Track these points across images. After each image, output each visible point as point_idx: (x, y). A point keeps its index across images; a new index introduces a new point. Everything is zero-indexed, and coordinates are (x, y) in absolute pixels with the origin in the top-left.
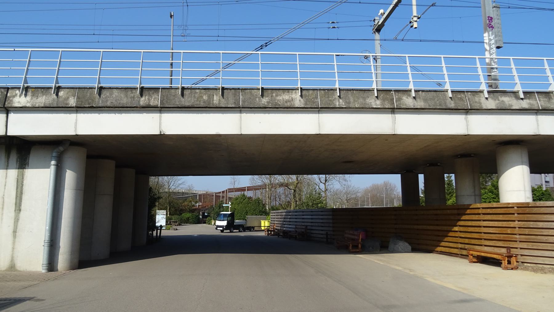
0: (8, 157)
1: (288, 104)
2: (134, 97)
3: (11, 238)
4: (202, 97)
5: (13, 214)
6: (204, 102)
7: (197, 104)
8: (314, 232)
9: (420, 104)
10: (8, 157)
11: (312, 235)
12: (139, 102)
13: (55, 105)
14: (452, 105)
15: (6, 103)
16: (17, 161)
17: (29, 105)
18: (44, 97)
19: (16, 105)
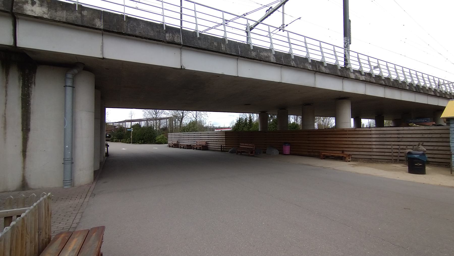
0: (7, 74)
1: (267, 59)
2: (159, 32)
3: (20, 158)
4: (213, 43)
5: (19, 134)
6: (215, 47)
7: (210, 48)
8: (210, 145)
9: (327, 71)
10: (7, 74)
11: (209, 147)
12: (165, 37)
13: (80, 23)
14: (340, 74)
15: (14, 8)
16: (19, 79)
17: (46, 16)
18: (65, 12)
19: (29, 13)
